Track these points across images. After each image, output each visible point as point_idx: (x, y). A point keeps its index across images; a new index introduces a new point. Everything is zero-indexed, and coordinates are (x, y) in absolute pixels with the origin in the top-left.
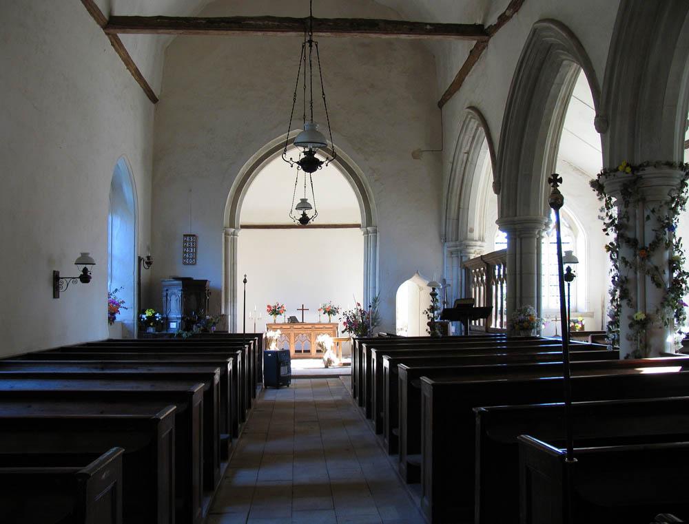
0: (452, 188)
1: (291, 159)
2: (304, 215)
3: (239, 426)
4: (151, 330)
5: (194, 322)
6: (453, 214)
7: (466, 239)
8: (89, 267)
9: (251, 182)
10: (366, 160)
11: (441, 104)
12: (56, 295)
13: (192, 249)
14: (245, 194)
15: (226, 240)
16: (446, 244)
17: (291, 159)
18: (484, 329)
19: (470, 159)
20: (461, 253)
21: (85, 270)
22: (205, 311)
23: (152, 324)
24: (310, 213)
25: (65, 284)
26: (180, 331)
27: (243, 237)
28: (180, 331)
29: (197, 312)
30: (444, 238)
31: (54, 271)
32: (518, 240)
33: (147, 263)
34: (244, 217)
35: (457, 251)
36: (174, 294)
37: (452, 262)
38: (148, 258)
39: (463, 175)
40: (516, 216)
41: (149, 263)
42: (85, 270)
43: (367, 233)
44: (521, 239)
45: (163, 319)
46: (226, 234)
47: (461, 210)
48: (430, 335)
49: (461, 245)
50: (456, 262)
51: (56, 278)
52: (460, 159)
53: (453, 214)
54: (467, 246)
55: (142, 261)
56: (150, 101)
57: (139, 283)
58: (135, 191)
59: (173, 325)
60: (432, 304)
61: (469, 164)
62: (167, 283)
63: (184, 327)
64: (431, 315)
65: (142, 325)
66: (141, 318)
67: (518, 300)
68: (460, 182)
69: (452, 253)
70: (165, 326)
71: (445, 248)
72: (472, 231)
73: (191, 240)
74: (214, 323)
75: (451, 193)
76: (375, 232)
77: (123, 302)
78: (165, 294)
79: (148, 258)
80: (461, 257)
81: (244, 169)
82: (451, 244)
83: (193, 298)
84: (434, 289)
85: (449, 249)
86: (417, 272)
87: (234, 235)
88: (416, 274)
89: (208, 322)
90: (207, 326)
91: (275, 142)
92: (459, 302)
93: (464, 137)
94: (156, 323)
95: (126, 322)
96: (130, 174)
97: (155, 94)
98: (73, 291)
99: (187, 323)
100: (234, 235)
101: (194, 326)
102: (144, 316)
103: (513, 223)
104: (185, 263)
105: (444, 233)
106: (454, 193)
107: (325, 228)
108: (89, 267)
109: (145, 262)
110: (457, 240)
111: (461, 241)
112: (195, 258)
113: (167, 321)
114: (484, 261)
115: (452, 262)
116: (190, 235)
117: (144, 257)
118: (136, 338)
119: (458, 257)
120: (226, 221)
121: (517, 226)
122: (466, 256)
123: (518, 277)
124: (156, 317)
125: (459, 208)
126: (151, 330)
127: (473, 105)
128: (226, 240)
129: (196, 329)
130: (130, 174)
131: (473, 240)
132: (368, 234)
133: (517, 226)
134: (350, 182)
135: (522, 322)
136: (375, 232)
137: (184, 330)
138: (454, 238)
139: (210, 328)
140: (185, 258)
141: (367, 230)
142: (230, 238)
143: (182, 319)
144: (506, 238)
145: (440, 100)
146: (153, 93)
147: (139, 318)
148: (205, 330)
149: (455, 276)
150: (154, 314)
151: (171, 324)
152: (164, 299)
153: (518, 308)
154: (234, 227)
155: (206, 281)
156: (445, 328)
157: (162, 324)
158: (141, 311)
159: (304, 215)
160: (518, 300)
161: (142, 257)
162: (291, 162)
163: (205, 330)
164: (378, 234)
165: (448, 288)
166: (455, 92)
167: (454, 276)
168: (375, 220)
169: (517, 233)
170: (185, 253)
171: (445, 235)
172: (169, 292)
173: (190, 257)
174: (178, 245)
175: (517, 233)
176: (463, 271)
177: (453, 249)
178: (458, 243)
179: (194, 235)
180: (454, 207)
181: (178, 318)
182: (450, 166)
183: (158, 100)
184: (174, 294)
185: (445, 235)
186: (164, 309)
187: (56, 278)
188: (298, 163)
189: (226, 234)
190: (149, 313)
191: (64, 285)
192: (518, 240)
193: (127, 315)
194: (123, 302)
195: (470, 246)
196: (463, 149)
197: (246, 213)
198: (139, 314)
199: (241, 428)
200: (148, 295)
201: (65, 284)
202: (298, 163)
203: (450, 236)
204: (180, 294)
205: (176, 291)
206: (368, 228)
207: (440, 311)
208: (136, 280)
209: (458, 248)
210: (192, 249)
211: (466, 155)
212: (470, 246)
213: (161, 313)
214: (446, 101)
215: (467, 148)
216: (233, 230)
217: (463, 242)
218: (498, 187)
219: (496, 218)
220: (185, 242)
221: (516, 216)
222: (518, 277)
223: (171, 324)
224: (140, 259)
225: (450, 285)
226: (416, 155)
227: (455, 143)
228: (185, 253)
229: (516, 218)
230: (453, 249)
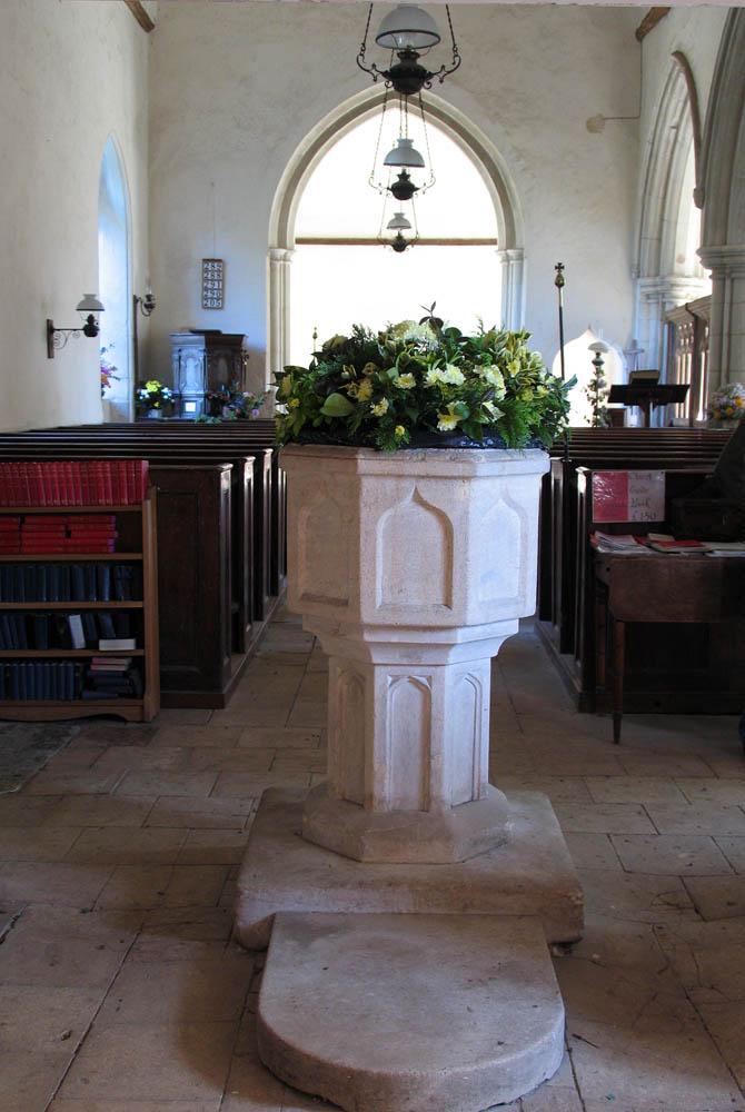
0: (652, 186)
1: (374, 66)
2: (404, 176)
3: (226, 661)
4: (155, 414)
5: (224, 403)
6: (652, 231)
7: (671, 273)
8: (95, 314)
9: (313, 169)
10: (508, 133)
11: (641, 34)
12: (50, 355)
13: (216, 283)
14: (303, 189)
15: (273, 270)
16: (640, 281)
17: (374, 66)
18: (687, 423)
19: (680, 138)
20: (663, 297)
21: (91, 319)
22: (240, 385)
23: (156, 405)
24: (416, 176)
25: (63, 337)
26: (203, 416)
27: (301, 258)
28: (203, 416)
29: (229, 385)
30: (636, 272)
31: (48, 321)
32: (728, 283)
33: (146, 306)
34: (301, 225)
35: (657, 293)
36: (193, 357)
37: (649, 312)
38: (149, 297)
39: (671, 158)
40: (725, 244)
41: (150, 307)
42: (91, 319)
43: (507, 259)
44: (733, 280)
45: (174, 396)
46: (273, 259)
47: (665, 223)
48: (590, 425)
49: (662, 284)
50: (654, 311)
51: (51, 330)
52: (664, 137)
53: (652, 231)
54: (672, 285)
55: (139, 304)
56: (138, 25)
57: (135, 339)
58: (125, 191)
59: (190, 407)
60: (595, 378)
61: (678, 146)
62: (181, 339)
63: (208, 410)
64: (593, 394)
65: (143, 407)
66: (140, 395)
67: (723, 374)
68: (664, 175)
69: (648, 296)
70: (177, 409)
71: (638, 287)
72: (681, 260)
73: (214, 268)
74: (256, 404)
75: (650, 194)
76: (520, 258)
77: (114, 369)
78: (176, 356)
79: (149, 297)
80: (664, 303)
81: (302, 147)
82: (649, 281)
83: (222, 364)
84: (598, 354)
85: (644, 290)
86: (590, 328)
87: (285, 260)
88: (588, 332)
89: (247, 402)
90: (246, 409)
91: (359, 99)
92: (634, 376)
93: (670, 100)
94: (164, 403)
95: (115, 401)
96: (119, 161)
97: (150, 16)
98: (73, 347)
99: (213, 404)
100: (285, 260)
101: (225, 408)
102: (144, 392)
103: (721, 255)
104: (205, 307)
105: (636, 262)
106: (654, 194)
107: (440, 244)
108: (95, 314)
109: (144, 304)
110: (657, 274)
111: (663, 278)
112: (221, 298)
113: (180, 400)
114: (690, 312)
115: (649, 312)
116: (213, 261)
117: (142, 295)
118: (131, 421)
119: (658, 303)
120: (273, 237)
121: (725, 260)
122: (672, 303)
123: (725, 338)
124: (164, 394)
125: (662, 220)
126: (155, 414)
127: (683, 49)
128: (273, 270)
129: (228, 413)
130: (119, 161)
131: (683, 276)
132: (508, 261)
133: (725, 260)
134: (481, 172)
135: (724, 407)
136: (520, 258)
137: (209, 415)
138: (652, 272)
139: (250, 411)
140: (205, 298)
141: (507, 255)
142: (278, 264)
143: (206, 396)
144: (710, 277)
145: (639, 25)
146: (147, 16)
147: (137, 396)
148: (242, 415)
149: (652, 336)
150: (160, 389)
151: (187, 405)
152: (176, 364)
153: (723, 387)
154: (285, 247)
155: (242, 336)
156: (617, 416)
157: (173, 405)
158: (140, 384)
159: (404, 176)
160: (723, 374)
161: (138, 296)
162: (373, 71)
163: (242, 415)
164: (525, 261)
165: (639, 355)
166: (660, 18)
167: (650, 335)
168: (522, 236)
169: (727, 271)
170: (206, 289)
171: (639, 265)
172: (184, 353)
173: (214, 297)
174: (194, 277)
175: (727, 271)
176: (666, 326)
177: (651, 289)
178: (658, 279)
179: (220, 261)
180: (653, 218)
181: (198, 396)
182: (648, 148)
183: (153, 26)
184: (193, 357)
185: (639, 265)
186: (176, 382)
187: (51, 330)
188: (385, 74)
189: (273, 259)
190: (152, 387)
191: (62, 341)
192: (728, 283)
193: (120, 391)
194: (114, 369)
195: (678, 285)
196: (669, 119)
197: (304, 221)
198: (136, 388)
199: (251, 630)
200: (149, 359)
201: (63, 337)
202: (385, 74)
203: (645, 266)
204: (201, 356)
205: (194, 352)
206: (509, 251)
207: (608, 388)
208: (131, 333)
209: (659, 289)
210: (216, 283)
211: (674, 131)
212: (678, 285)
213: (171, 388)
214: (648, 31)
215: (676, 119)
216: (282, 252)
217: (667, 279)
218: (701, 198)
219: (698, 246)
220: (206, 270)
221: (725, 244)
222: (725, 338)
223: (187, 405)
224: (136, 301)
225: (643, 351)
226: (593, 126)
227: (656, 109)
228: (206, 289)
229: (725, 248)
230: (651, 289)
